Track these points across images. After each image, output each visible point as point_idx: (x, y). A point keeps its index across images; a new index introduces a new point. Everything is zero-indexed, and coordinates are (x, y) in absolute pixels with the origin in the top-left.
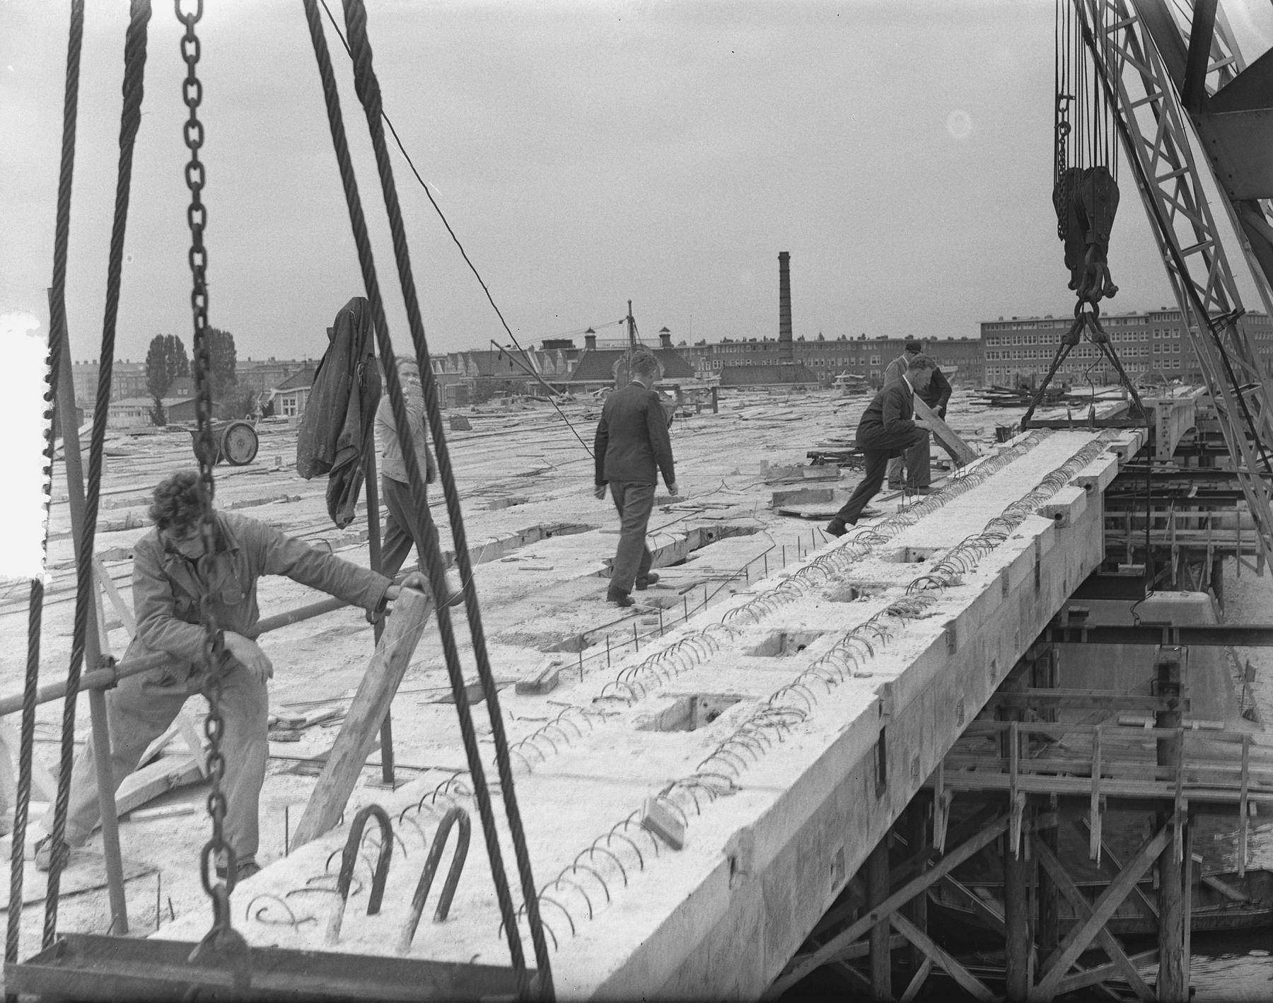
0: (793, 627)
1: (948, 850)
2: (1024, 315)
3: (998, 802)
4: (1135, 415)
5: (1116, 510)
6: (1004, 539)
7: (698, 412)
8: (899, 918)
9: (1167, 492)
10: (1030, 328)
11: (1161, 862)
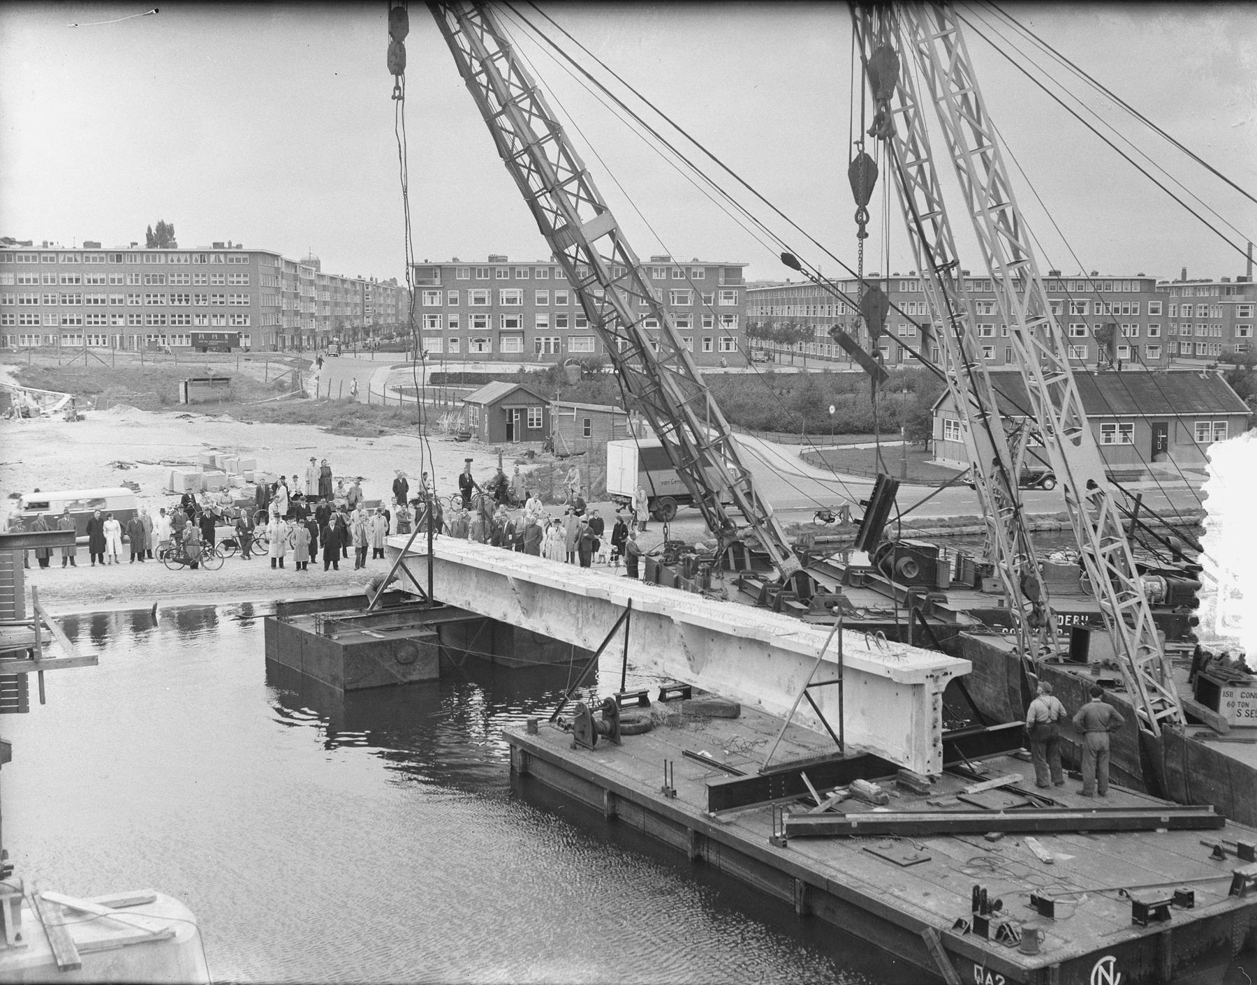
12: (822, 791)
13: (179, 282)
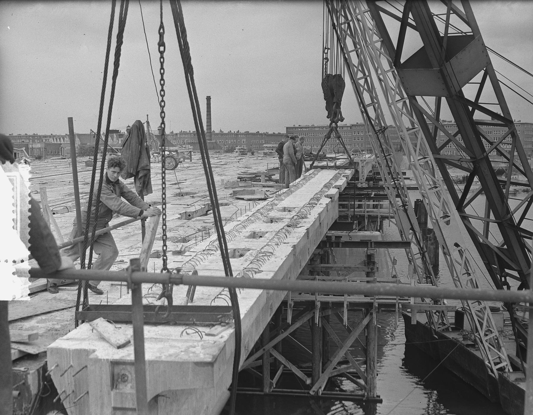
0: (257, 230)
1: (292, 324)
2: (303, 124)
3: (311, 305)
4: (352, 164)
5: (344, 201)
6: (316, 204)
7: (184, 161)
8: (273, 350)
9: (363, 194)
10: (306, 129)
11: (367, 326)
12: (525, 347)
13: (497, 133)
